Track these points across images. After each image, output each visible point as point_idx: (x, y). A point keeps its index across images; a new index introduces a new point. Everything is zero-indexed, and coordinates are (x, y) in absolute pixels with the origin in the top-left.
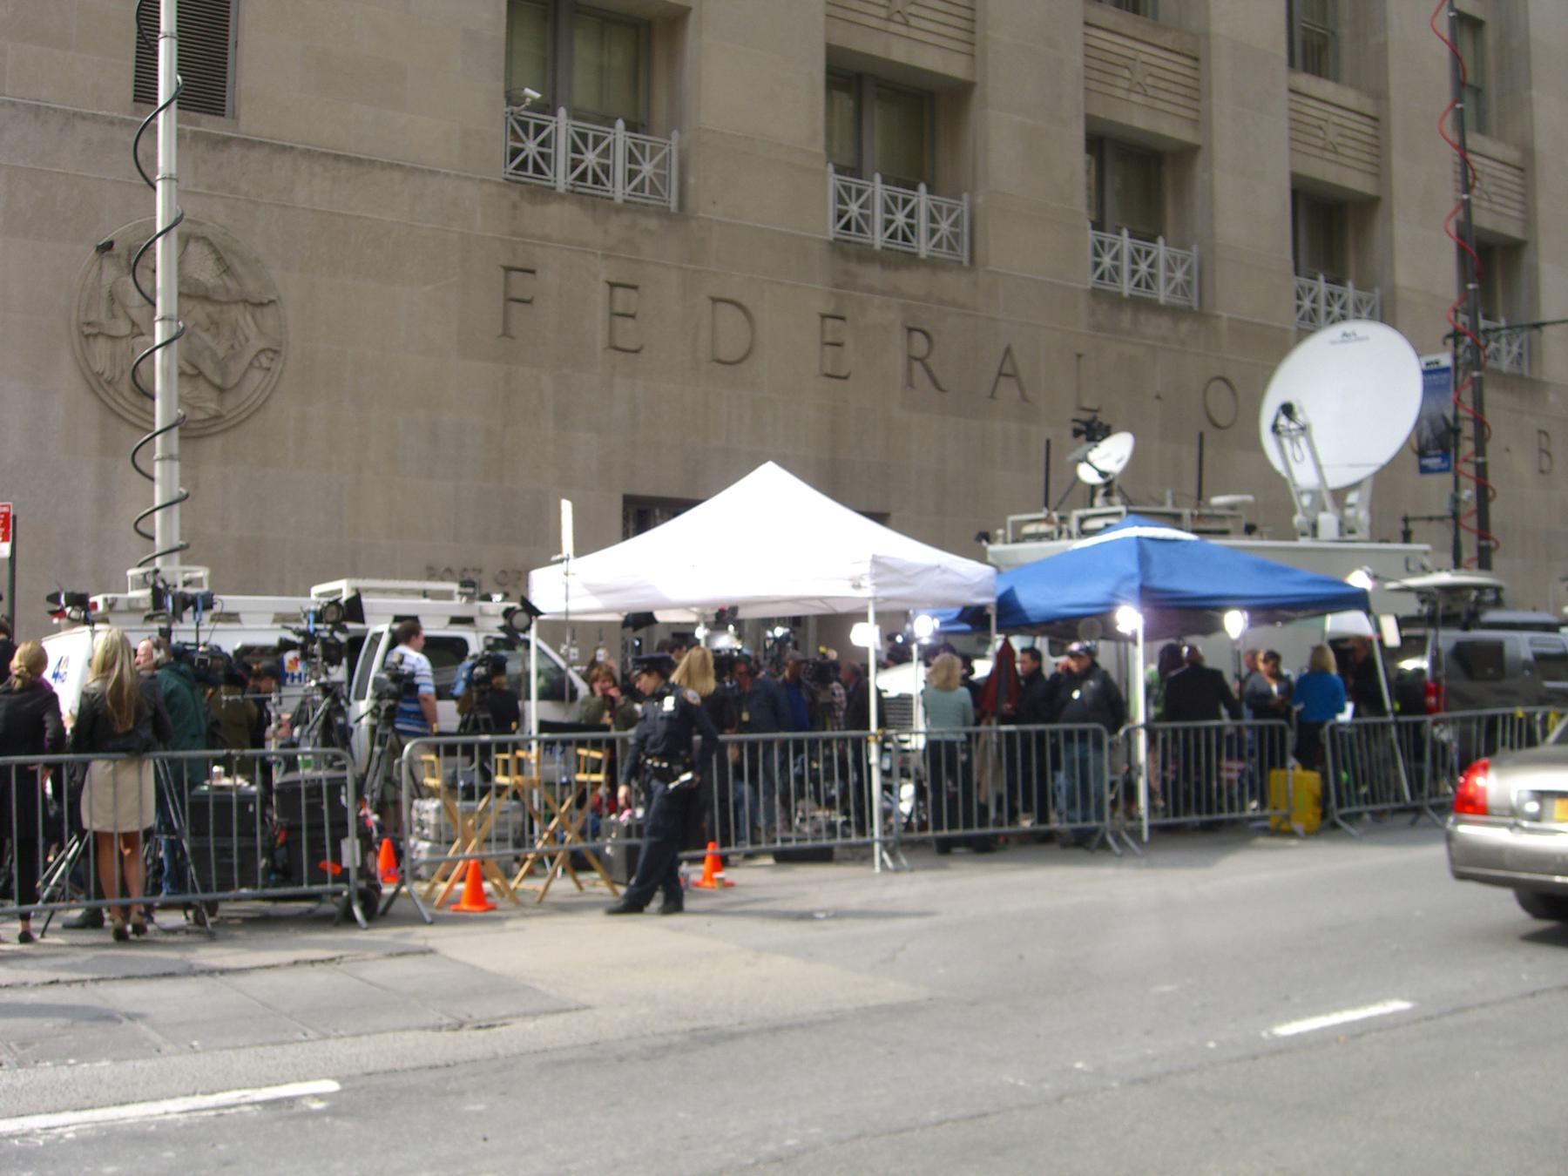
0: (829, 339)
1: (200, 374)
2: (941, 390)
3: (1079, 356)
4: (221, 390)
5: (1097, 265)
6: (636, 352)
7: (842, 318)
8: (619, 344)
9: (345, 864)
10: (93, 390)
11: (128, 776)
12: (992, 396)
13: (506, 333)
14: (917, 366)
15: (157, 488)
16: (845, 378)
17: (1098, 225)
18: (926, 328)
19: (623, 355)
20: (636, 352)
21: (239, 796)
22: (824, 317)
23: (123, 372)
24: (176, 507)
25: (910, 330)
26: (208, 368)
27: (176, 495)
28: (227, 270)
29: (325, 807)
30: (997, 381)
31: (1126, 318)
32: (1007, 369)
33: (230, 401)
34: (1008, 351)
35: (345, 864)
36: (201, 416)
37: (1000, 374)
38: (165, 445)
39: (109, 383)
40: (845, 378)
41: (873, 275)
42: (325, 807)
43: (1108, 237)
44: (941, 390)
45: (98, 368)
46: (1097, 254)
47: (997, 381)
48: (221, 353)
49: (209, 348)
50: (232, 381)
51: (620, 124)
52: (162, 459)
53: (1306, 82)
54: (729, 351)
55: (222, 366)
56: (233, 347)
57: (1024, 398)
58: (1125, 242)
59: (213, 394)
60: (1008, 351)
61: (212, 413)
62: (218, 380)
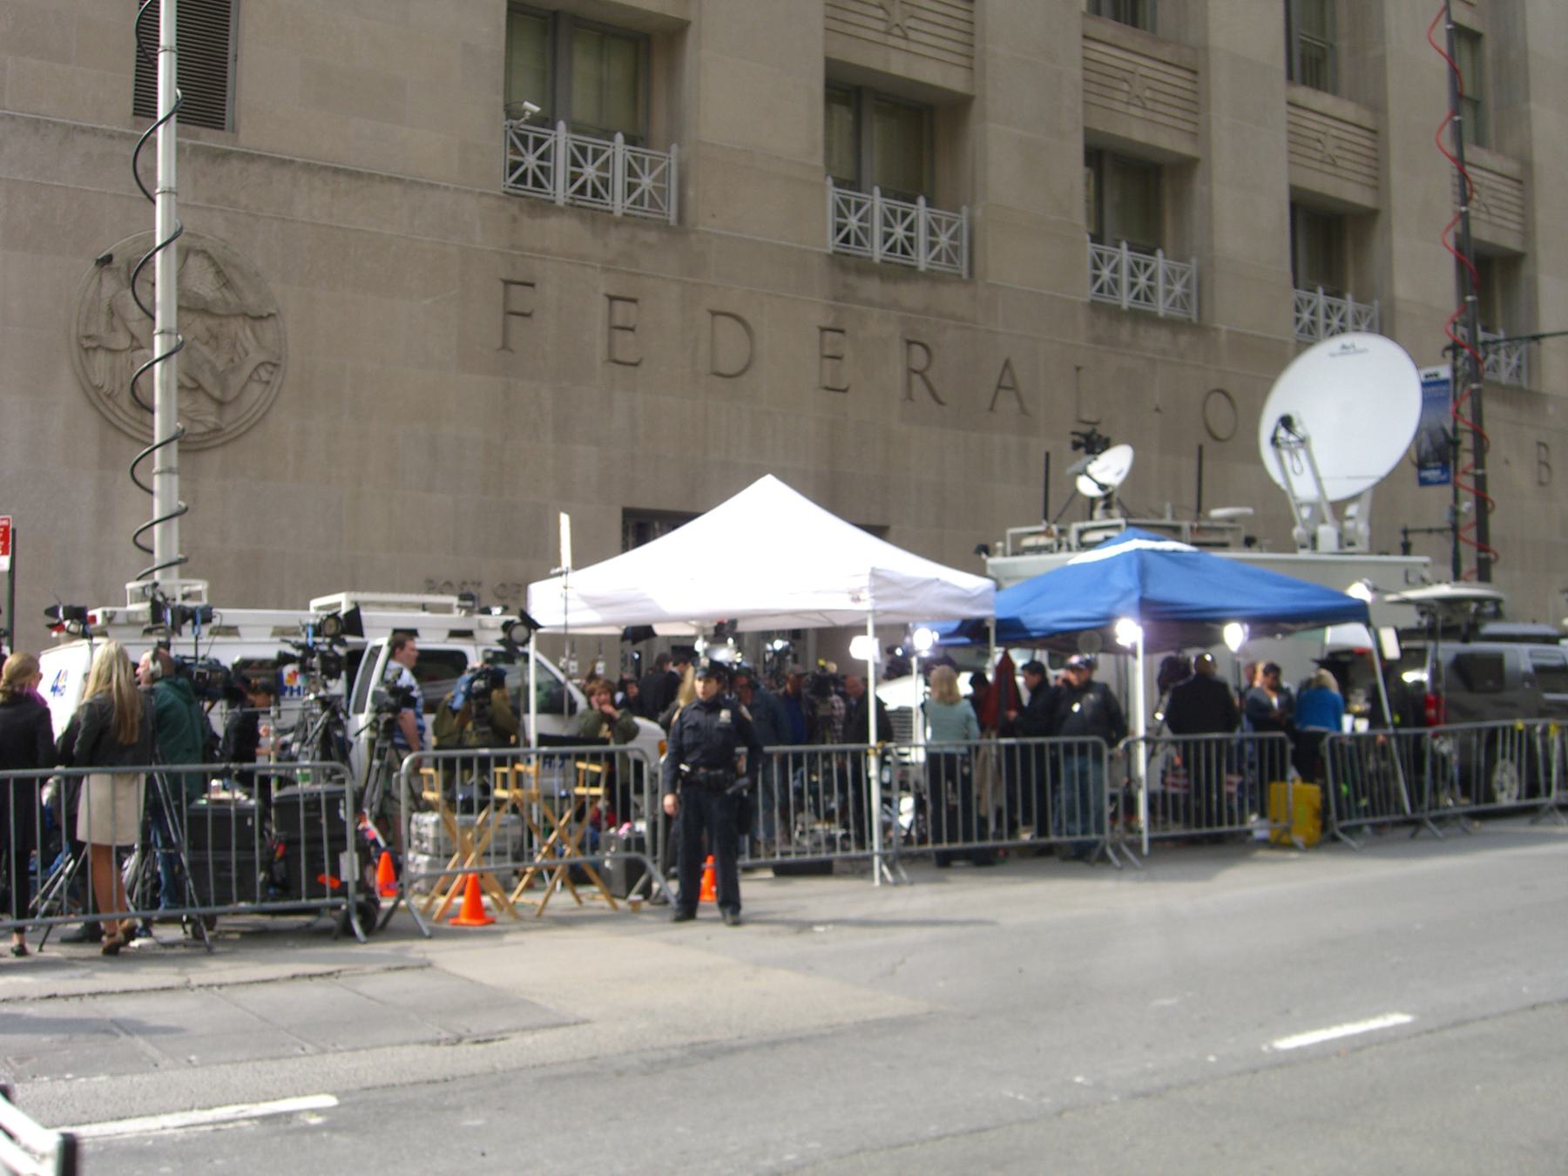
0: (828, 352)
1: (199, 387)
2: (940, 403)
3: (1078, 369)
4: (221, 404)
5: (1096, 278)
6: (635, 365)
7: (842, 331)
10: (92, 403)
13: (505, 346)
14: (916, 378)
16: (845, 391)
17: (1097, 238)
20: (635, 365)
23: (122, 386)
24: (175, 521)
25: (909, 343)
26: (207, 380)
27: (175, 509)
28: (227, 284)
29: (324, 821)
31: (1125, 331)
32: (1007, 382)
33: (230, 414)
34: (1007, 364)
36: (200, 429)
37: (1000, 387)
38: (164, 459)
39: (109, 396)
40: (845, 391)
41: (872, 288)
42: (324, 821)
43: (1107, 250)
44: (940, 403)
45: (97, 382)
46: (1096, 267)
48: (220, 367)
49: (209, 362)
50: (231, 395)
51: (619, 137)
52: (161, 472)
53: (1304, 94)
55: (221, 378)
56: (232, 360)
57: (1023, 411)
58: (1124, 255)
60: (1007, 364)
62: (217, 393)
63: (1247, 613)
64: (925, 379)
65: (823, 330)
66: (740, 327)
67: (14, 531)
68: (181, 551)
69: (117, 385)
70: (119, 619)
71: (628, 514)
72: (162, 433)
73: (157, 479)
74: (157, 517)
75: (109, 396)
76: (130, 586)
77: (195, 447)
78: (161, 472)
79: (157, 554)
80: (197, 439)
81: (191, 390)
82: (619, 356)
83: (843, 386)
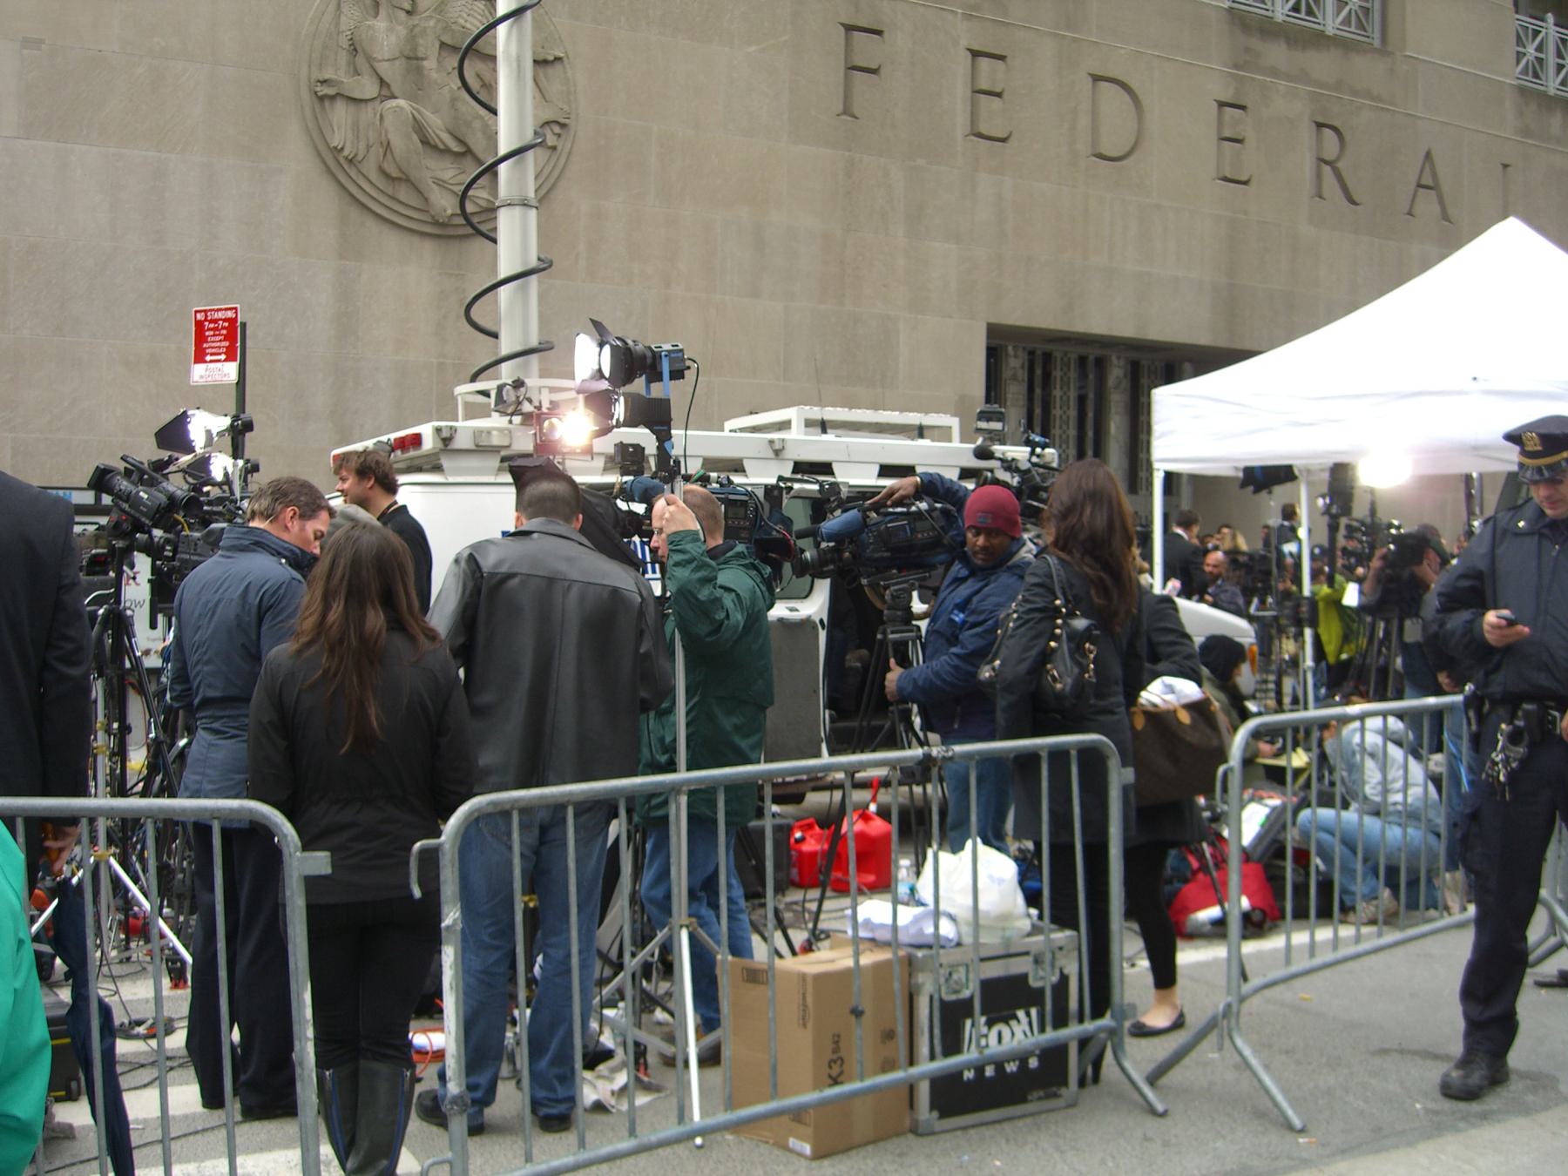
0: (1227, 134)
2: (1354, 203)
3: (1505, 166)
6: (1003, 140)
7: (1243, 108)
13: (847, 111)
14: (1327, 169)
18: (1336, 123)
20: (1003, 140)
22: (1222, 104)
23: (368, 147)
25: (1320, 125)
32: (1427, 180)
34: (1428, 156)
37: (1420, 186)
39: (351, 161)
40: (1245, 183)
44: (1354, 203)
45: (336, 141)
57: (1445, 216)
60: (1428, 156)
61: (483, 204)
65: (1222, 104)
67: (244, 325)
69: (362, 146)
70: (461, 442)
71: (999, 343)
75: (351, 161)
83: (1244, 178)
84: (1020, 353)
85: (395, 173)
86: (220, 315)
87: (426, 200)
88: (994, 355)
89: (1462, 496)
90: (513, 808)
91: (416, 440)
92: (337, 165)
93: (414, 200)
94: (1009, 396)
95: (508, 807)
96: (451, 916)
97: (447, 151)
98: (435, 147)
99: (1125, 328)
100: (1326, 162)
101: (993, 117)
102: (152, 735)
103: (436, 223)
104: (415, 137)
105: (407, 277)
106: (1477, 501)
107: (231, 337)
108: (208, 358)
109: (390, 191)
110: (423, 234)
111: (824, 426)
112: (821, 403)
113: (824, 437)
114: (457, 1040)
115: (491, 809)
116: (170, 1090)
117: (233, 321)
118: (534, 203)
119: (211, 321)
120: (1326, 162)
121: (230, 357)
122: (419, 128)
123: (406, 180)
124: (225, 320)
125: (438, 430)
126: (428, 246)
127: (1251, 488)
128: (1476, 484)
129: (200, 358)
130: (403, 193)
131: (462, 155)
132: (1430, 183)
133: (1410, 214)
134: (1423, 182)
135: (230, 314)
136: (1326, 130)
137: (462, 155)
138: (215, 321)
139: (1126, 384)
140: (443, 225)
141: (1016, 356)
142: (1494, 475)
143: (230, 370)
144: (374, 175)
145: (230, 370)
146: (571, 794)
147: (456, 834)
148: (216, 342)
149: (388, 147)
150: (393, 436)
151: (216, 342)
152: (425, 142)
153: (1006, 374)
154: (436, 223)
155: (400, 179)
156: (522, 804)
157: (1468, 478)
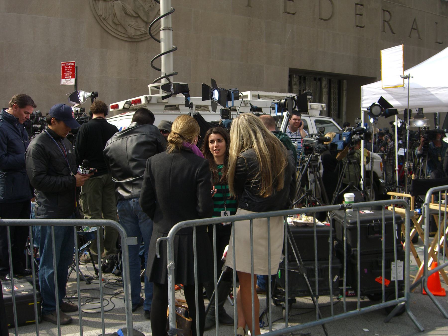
0: (358, 13)
1: (139, 16)
2: (393, 33)
3: (437, 23)
6: (293, 14)
7: (362, 5)
8: (288, 11)
9: (392, 279)
10: (98, 22)
11: (260, 224)
12: (410, 37)
13: (249, 5)
14: (386, 23)
15: (162, 44)
16: (363, 27)
19: (290, 15)
20: (293, 14)
21: (318, 232)
22: (356, 4)
23: (109, 15)
24: (171, 53)
25: (384, 11)
26: (142, 14)
27: (171, 49)
29: (383, 239)
30: (411, 31)
32: (414, 27)
34: (415, 20)
35: (392, 279)
36: (139, 33)
37: (412, 29)
38: (165, 23)
39: (104, 19)
40: (363, 27)
42: (383, 239)
44: (393, 33)
45: (100, 13)
47: (411, 31)
48: (146, 8)
49: (142, 6)
52: (164, 30)
54: (325, 15)
55: (147, 13)
56: (151, 6)
57: (420, 38)
59: (143, 25)
60: (415, 20)
61: (143, 32)
62: (145, 19)
63: (254, 129)
64: (389, 24)
65: (356, 4)
66: (155, 66)
67: (77, 67)
68: (174, 69)
69: (107, 15)
70: (153, 101)
71: (292, 72)
72: (164, 10)
73: (162, 33)
74: (162, 51)
75: (104, 19)
76: (149, 86)
77: (137, 40)
78: (164, 30)
79: (163, 70)
80: (138, 37)
81: (135, 17)
82: (288, 11)
84: (297, 77)
85: (117, 23)
86: (69, 64)
87: (126, 31)
88: (290, 77)
89: (433, 120)
90: (193, 226)
91: (139, 101)
92: (100, 20)
93: (123, 31)
94: (294, 89)
95: (192, 225)
96: (170, 264)
97: (132, 16)
98: (129, 15)
99: (328, 70)
100: (386, 21)
101: (291, 7)
102: (224, 224)
103: (129, 38)
104: (123, 12)
105: (120, 53)
106: (438, 120)
107: (73, 71)
108: (66, 77)
109: (116, 28)
110: (126, 41)
111: (259, 97)
112: (257, 90)
113: (259, 100)
114: (173, 308)
115: (185, 226)
116: (84, 333)
117: (73, 66)
118: (171, 29)
119: (67, 66)
120: (386, 21)
121: (73, 77)
122: (124, 9)
123: (121, 25)
124: (71, 66)
125: (146, 98)
126: (127, 44)
127: (384, 117)
128: (438, 115)
129: (63, 77)
130: (120, 29)
131: (137, 17)
132: (416, 28)
133: (410, 37)
134: (414, 27)
135: (72, 64)
136: (386, 12)
137: (137, 17)
138: (68, 66)
139: (327, 86)
140: (131, 38)
141: (296, 78)
142: (443, 113)
143: (73, 81)
144: (111, 23)
145: (73, 81)
146: (214, 220)
147: (173, 235)
148: (68, 72)
149: (115, 15)
150: (131, 100)
151: (68, 72)
152: (126, 13)
153: (293, 83)
154: (129, 38)
155: (119, 25)
156: (197, 224)
157: (435, 114)
